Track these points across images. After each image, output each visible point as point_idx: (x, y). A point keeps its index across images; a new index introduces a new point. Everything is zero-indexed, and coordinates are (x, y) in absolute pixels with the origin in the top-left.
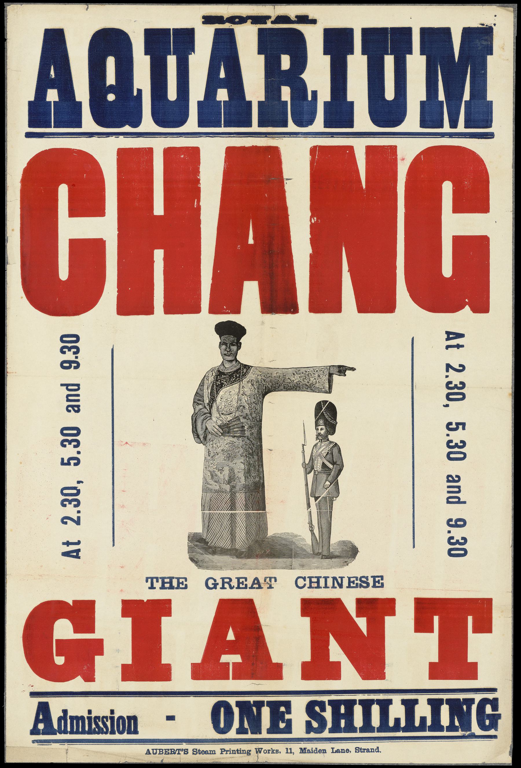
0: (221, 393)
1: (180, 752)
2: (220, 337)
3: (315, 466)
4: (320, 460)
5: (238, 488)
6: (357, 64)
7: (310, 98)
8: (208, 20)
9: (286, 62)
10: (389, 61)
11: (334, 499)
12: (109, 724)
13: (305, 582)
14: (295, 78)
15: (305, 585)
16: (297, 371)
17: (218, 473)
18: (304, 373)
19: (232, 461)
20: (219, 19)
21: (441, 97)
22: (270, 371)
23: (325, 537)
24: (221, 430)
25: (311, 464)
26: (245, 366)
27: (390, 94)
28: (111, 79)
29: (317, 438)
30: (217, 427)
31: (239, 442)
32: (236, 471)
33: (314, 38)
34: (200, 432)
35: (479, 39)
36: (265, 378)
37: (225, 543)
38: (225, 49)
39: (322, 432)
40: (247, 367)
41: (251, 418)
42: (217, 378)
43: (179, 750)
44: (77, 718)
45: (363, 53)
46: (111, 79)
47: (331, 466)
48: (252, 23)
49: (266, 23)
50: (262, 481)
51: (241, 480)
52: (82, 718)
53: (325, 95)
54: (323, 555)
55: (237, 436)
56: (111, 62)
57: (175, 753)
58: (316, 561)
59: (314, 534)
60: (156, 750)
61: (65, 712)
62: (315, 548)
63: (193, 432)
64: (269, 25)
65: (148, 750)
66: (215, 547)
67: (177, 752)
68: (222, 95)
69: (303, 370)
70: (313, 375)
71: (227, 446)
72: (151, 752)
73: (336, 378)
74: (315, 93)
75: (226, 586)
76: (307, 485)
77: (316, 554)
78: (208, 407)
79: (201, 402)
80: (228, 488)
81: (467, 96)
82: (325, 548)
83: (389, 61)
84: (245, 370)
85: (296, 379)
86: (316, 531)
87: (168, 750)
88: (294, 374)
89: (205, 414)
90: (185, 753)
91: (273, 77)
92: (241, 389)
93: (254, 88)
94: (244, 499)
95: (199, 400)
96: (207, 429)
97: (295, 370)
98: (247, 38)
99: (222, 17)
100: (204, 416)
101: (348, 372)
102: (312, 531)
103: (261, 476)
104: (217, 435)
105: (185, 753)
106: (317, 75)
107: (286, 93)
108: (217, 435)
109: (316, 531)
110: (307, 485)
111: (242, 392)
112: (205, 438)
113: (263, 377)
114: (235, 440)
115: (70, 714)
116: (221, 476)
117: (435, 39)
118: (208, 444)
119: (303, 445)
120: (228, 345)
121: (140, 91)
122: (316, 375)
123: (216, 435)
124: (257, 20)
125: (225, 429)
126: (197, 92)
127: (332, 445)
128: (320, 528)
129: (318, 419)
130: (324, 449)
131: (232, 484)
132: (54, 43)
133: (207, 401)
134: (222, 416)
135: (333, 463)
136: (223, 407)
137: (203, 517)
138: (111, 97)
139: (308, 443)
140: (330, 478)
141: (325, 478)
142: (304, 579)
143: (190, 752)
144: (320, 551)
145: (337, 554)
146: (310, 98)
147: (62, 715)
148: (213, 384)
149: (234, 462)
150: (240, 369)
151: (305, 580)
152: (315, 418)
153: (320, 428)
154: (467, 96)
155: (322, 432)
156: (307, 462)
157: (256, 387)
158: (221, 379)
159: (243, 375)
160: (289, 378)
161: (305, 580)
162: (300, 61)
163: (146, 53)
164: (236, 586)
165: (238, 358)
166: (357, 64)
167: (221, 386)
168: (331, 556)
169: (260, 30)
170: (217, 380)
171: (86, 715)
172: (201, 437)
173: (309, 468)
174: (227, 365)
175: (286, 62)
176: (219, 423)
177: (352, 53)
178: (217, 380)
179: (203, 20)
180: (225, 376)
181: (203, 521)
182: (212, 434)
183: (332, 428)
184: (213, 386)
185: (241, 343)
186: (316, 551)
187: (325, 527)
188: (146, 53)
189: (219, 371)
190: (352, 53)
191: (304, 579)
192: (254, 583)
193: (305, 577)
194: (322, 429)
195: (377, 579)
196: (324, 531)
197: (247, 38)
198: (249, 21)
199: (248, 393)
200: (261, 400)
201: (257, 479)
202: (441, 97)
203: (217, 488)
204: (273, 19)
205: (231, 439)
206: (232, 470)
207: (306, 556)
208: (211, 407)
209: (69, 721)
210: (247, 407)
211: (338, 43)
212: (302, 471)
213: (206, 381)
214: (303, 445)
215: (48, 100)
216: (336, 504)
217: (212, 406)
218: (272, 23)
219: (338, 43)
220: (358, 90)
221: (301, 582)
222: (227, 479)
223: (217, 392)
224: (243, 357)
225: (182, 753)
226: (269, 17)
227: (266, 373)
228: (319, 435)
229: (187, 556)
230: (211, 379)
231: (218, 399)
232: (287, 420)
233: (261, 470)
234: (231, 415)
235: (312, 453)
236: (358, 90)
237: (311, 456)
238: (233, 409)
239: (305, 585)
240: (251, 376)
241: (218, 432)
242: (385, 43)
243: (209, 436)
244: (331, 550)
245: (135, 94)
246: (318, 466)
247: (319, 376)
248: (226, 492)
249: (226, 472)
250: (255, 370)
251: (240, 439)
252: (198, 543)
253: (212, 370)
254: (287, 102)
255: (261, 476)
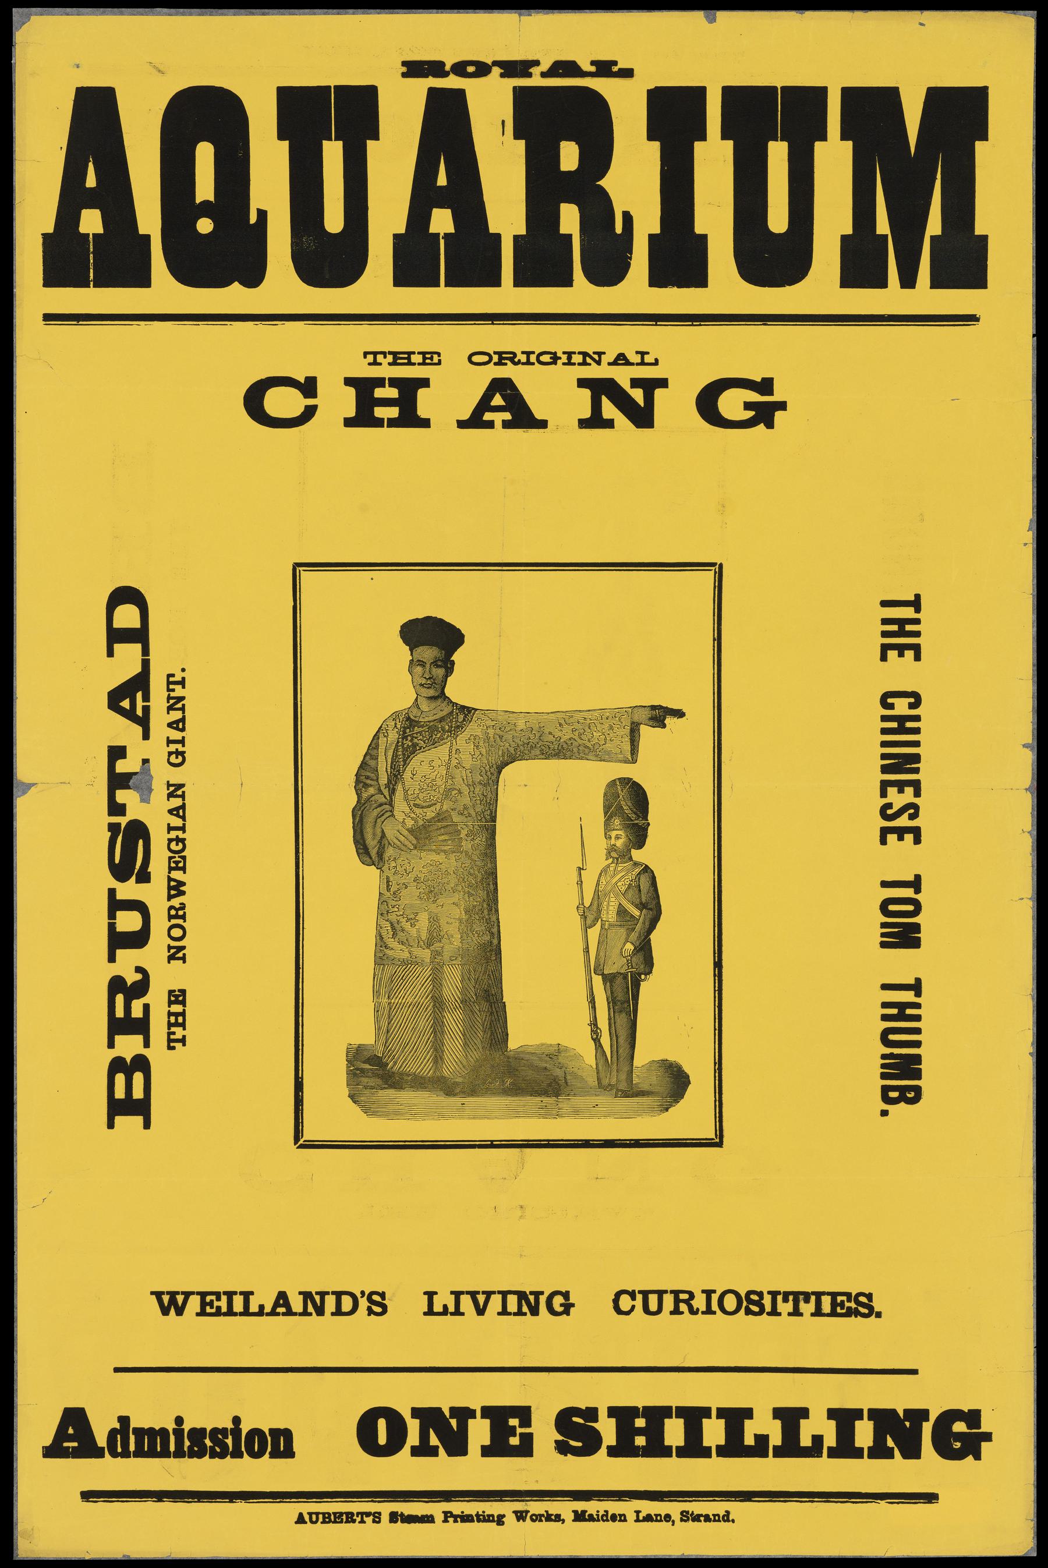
0: (414, 762)
1: (365, 1519)
2: (411, 650)
3: (604, 912)
4: (613, 899)
5: (446, 955)
6: (714, 161)
7: (619, 229)
8: (414, 69)
9: (569, 156)
10: (778, 153)
11: (643, 977)
12: (229, 1441)
13: (634, 1303)
14: (587, 188)
15: (633, 1307)
16: (566, 718)
17: (407, 926)
18: (582, 721)
19: (434, 902)
20: (435, 69)
21: (883, 226)
22: (512, 718)
23: (624, 1051)
24: (411, 838)
25: (595, 907)
26: (463, 708)
27: (778, 220)
28: (205, 189)
29: (609, 855)
30: (406, 833)
31: (451, 863)
32: (443, 922)
33: (627, 108)
34: (372, 843)
35: (960, 113)
36: (501, 733)
37: (420, 1064)
38: (446, 126)
39: (619, 843)
40: (467, 711)
41: (473, 814)
42: (405, 732)
43: (362, 1514)
44: (151, 1432)
45: (725, 136)
46: (205, 189)
47: (636, 912)
48: (502, 76)
49: (530, 75)
50: (495, 942)
51: (454, 941)
52: (164, 1432)
53: (648, 222)
54: (618, 1090)
55: (445, 851)
56: (205, 154)
57: (354, 1521)
58: (605, 1101)
59: (601, 1046)
60: (317, 1514)
61: (124, 1420)
62: (602, 1075)
63: (356, 842)
64: (536, 81)
65: (301, 1515)
66: (402, 1074)
67: (359, 1519)
68: (442, 221)
69: (578, 716)
70: (599, 725)
71: (425, 870)
72: (307, 1518)
73: (646, 732)
74: (627, 217)
75: (683, 1307)
76: (587, 950)
77: (603, 1087)
78: (386, 792)
79: (372, 782)
80: (426, 954)
81: (934, 226)
82: (623, 1076)
83: (778, 153)
84: (461, 717)
85: (566, 734)
86: (606, 1041)
87: (218, 1295)
88: (560, 725)
89: (381, 805)
90: (374, 1521)
91: (545, 187)
92: (454, 755)
93: (506, 213)
94: (459, 978)
95: (368, 778)
96: (383, 835)
97: (563, 715)
98: (490, 105)
99: (442, 64)
100: (379, 809)
101: (669, 721)
102: (597, 1041)
103: (495, 930)
104: (403, 848)
105: (374, 1521)
106: (633, 182)
107: (570, 219)
108: (403, 848)
109: (606, 1041)
110: (587, 950)
111: (454, 762)
112: (380, 855)
113: (498, 731)
114: (441, 858)
115: (133, 1424)
116: (413, 932)
117: (871, 112)
118: (387, 865)
119: (580, 869)
120: (428, 666)
121: (262, 214)
122: (606, 726)
123: (401, 848)
124: (512, 69)
125: (421, 835)
126: (388, 215)
127: (638, 870)
128: (614, 1035)
129: (611, 817)
130: (623, 877)
131: (437, 946)
132: (95, 115)
133: (383, 780)
134: (418, 811)
135: (641, 906)
136: (417, 791)
137: (376, 1011)
138: (205, 226)
139: (589, 866)
140: (634, 936)
141: (624, 936)
142: (632, 1295)
143: (385, 1518)
144: (614, 1081)
145: (645, 1087)
146: (619, 229)
147: (118, 1426)
148: (397, 746)
149: (440, 902)
150: (452, 712)
151: (633, 1298)
152: (606, 813)
153: (613, 834)
154: (934, 226)
155: (619, 843)
156: (587, 904)
157: (484, 751)
158: (410, 734)
159: (458, 727)
160: (550, 733)
161: (633, 1298)
162: (599, 154)
163: (281, 137)
164: (703, 1308)
165: (448, 692)
166: (714, 161)
167: (414, 750)
168: (632, 1092)
169: (518, 92)
170: (405, 738)
171: (171, 1426)
172: (373, 853)
173: (589, 915)
174: (424, 705)
175: (569, 156)
176: (410, 823)
177: (703, 138)
178: (405, 738)
179: (404, 69)
180: (421, 729)
181: (377, 1020)
182: (395, 846)
183: (639, 836)
184: (396, 750)
185: (453, 663)
186: (605, 1082)
187: (623, 1034)
188: (281, 137)
189: (408, 719)
190: (703, 138)
191: (632, 1295)
192: (178, 815)
193: (634, 1291)
194: (617, 837)
195: (839, 1299)
196: (621, 1040)
197: (490, 105)
198: (496, 71)
199: (468, 763)
200: (494, 778)
201: (487, 938)
202: (883, 226)
203: (406, 955)
204: (545, 66)
205: (434, 857)
206: (434, 920)
207: (586, 1091)
208: (393, 792)
209: (132, 1438)
210: (465, 790)
211: (675, 115)
212: (577, 921)
213: (382, 741)
214: (580, 869)
215: (433, 229)
216: (646, 988)
217: (394, 790)
218: (544, 75)
219: (675, 115)
220: (714, 214)
221: (625, 1302)
222: (424, 936)
223: (405, 761)
224: (457, 689)
225: (369, 1520)
226: (537, 63)
227: (502, 724)
228: (611, 850)
229: (346, 1092)
230: (393, 736)
231: (407, 775)
232: (548, 819)
233: (494, 918)
234: (433, 808)
235: (598, 884)
236: (714, 214)
237: (597, 891)
238: (436, 796)
239: (633, 1307)
240: (474, 728)
241: (407, 843)
242: (770, 116)
243: (390, 852)
244: (635, 1080)
245: (253, 218)
246: (610, 914)
247: (611, 728)
248: (421, 963)
249: (423, 920)
250: (483, 717)
251: (452, 856)
252: (367, 1066)
253: (395, 716)
254: (569, 237)
255: (495, 930)
